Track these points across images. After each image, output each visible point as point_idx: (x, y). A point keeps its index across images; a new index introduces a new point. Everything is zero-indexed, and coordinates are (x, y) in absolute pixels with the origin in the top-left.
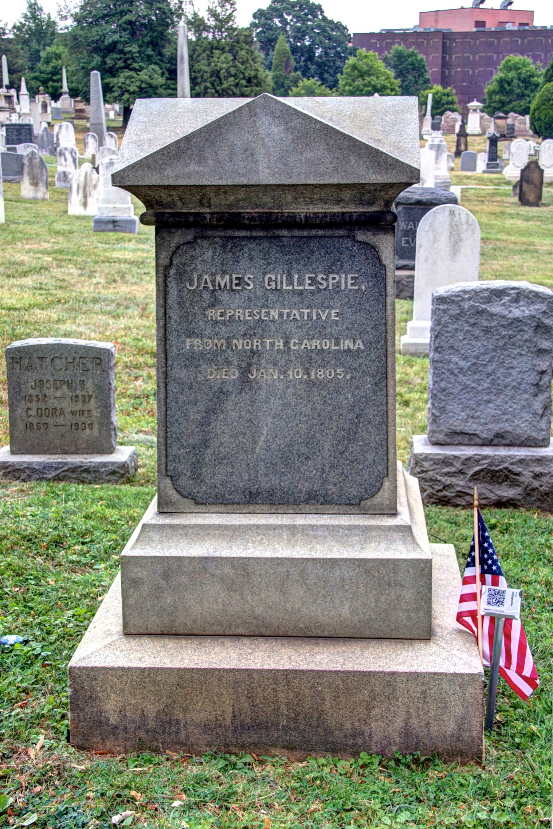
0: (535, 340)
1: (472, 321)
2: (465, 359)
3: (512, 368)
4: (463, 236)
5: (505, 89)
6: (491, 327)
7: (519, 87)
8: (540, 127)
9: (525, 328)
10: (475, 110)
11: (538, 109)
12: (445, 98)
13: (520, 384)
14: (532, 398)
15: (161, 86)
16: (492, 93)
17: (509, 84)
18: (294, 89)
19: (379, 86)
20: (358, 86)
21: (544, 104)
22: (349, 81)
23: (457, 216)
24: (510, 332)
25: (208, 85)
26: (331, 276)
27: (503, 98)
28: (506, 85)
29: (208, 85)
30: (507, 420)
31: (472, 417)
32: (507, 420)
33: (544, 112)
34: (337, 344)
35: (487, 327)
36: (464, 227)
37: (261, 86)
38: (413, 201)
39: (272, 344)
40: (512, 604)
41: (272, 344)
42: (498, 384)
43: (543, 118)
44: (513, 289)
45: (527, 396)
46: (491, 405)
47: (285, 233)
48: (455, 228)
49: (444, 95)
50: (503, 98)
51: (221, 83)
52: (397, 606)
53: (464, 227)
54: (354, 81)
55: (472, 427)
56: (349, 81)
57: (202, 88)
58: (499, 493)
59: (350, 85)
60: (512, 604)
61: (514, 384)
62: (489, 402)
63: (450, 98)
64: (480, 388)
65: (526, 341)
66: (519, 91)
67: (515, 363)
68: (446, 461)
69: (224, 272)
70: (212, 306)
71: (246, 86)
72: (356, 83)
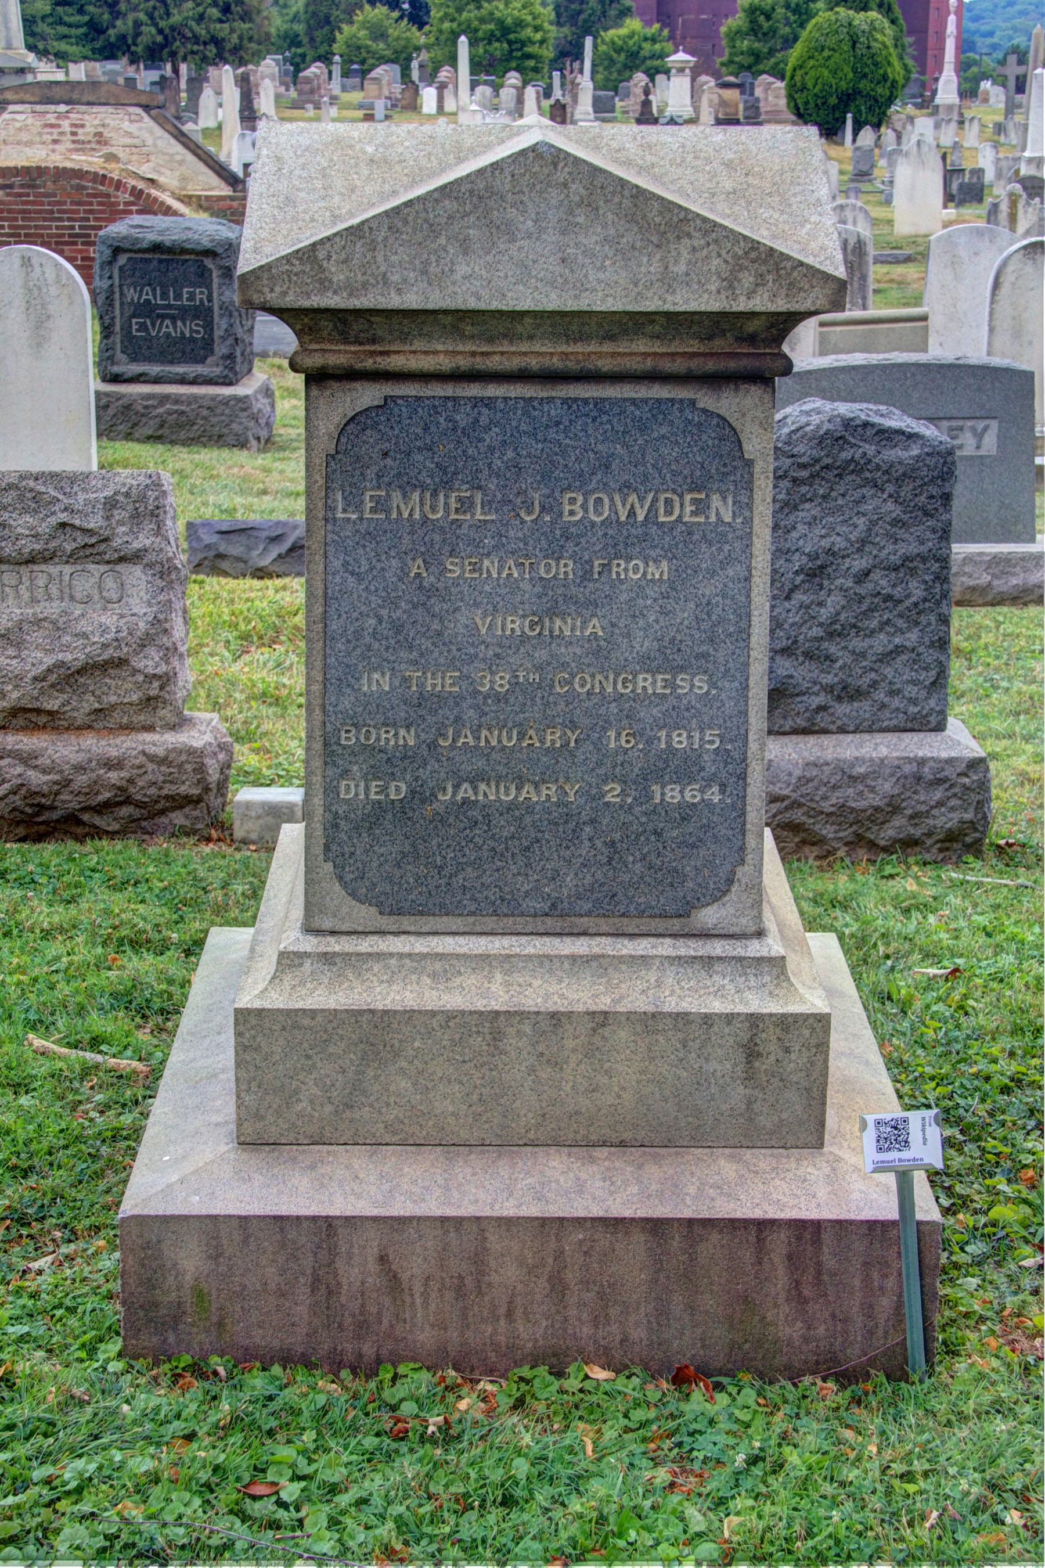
4: (52, 308)
5: (761, 27)
7: (788, 23)
8: (807, 103)
10: (681, 70)
11: (801, 67)
12: (647, 46)
15: (44, 18)
16: (735, 35)
17: (768, 18)
18: (345, 27)
19: (509, 20)
20: (469, 21)
21: (811, 57)
22: (451, 10)
23: (38, 270)
25: (142, 16)
27: (756, 45)
28: (762, 18)
29: (142, 16)
33: (812, 73)
36: (54, 291)
37: (251, 20)
38: (145, 245)
43: (810, 85)
48: (36, 292)
49: (646, 39)
50: (756, 45)
51: (168, 14)
52: (775, 1079)
53: (54, 291)
54: (459, 10)
56: (451, 10)
57: (130, 23)
59: (452, 20)
63: (657, 46)
66: (787, 30)
71: (221, 21)
72: (465, 14)
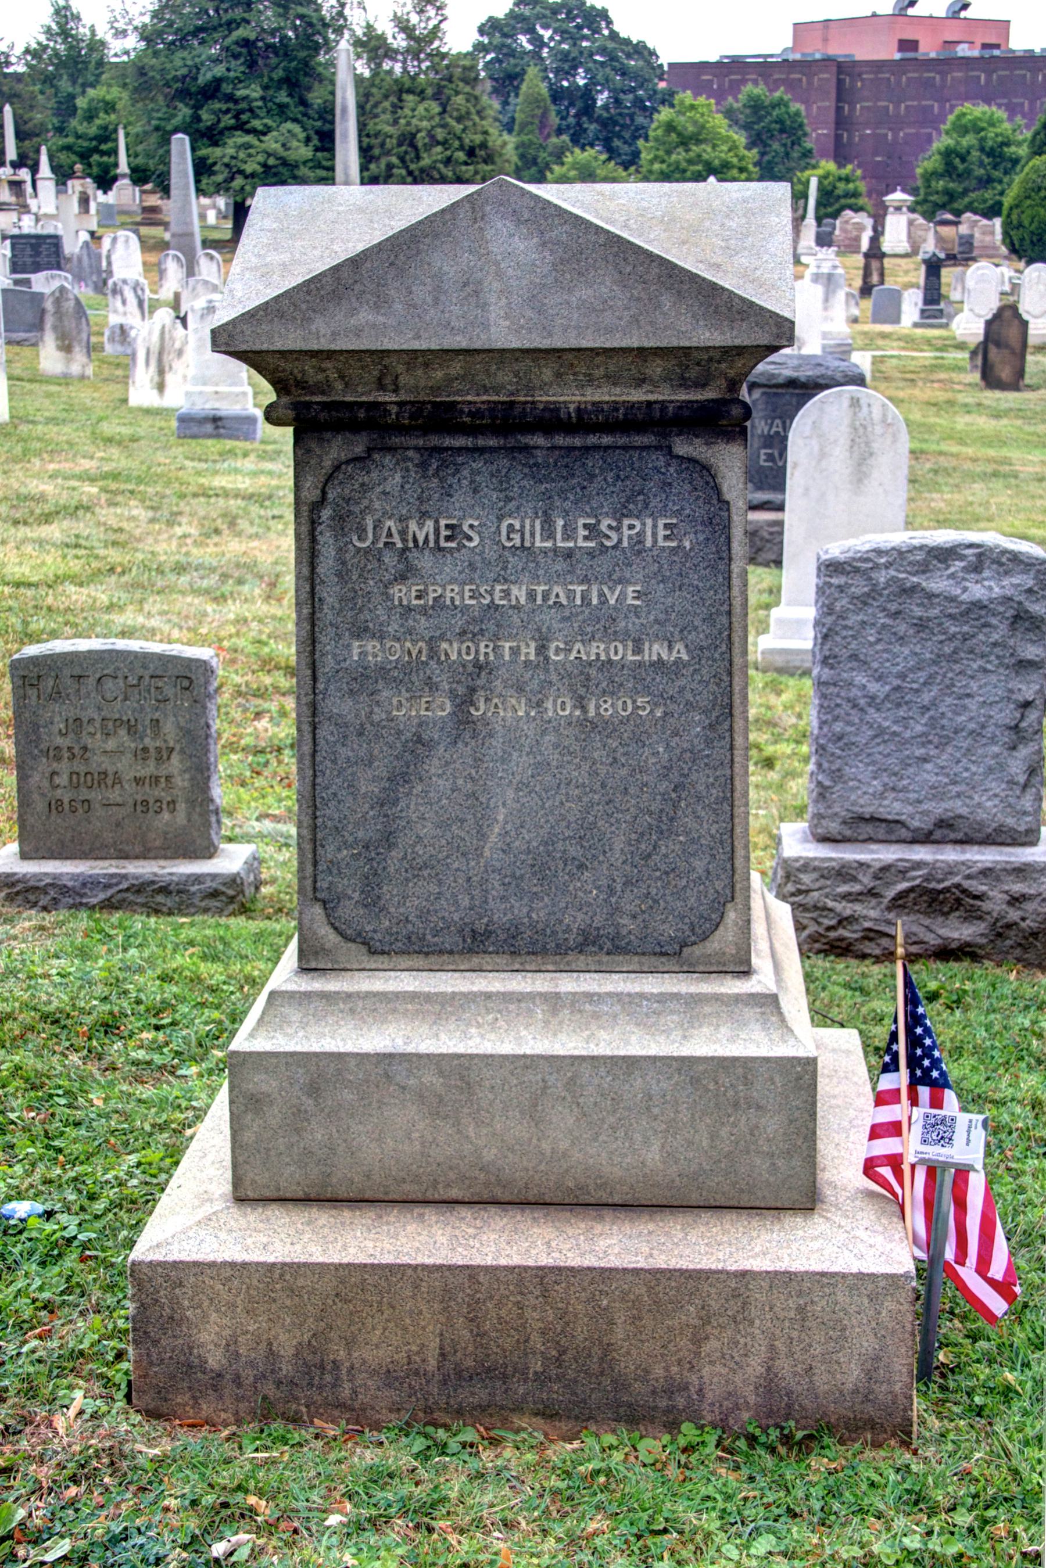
0: (1011, 642)
1: (893, 607)
2: (879, 679)
3: (968, 695)
4: (875, 446)
5: (955, 168)
6: (929, 619)
7: (981, 164)
8: (1022, 240)
9: (994, 621)
10: (898, 209)
11: (1017, 206)
12: (841, 186)
13: (983, 727)
14: (1006, 753)
15: (305, 163)
16: (930, 176)
17: (963, 160)
18: (556, 168)
19: (717, 162)
20: (678, 163)
21: (1028, 197)
22: (661, 153)
23: (865, 409)
24: (965, 628)
25: (394, 160)
26: (626, 522)
27: (951, 185)
28: (957, 161)
29: (394, 160)
30: (958, 795)
31: (893, 789)
32: (958, 795)
33: (1029, 212)
34: (638, 650)
35: (920, 619)
36: (879, 429)
37: (493, 163)
38: (781, 380)
39: (515, 651)
41: (515, 651)
42: (943, 727)
43: (1026, 223)
44: (971, 546)
45: (996, 749)
46: (929, 766)
47: (539, 440)
48: (861, 431)
49: (840, 179)
50: (951, 185)
51: (418, 158)
52: (752, 1146)
53: (879, 429)
54: (669, 153)
55: (893, 807)
56: (661, 153)
57: (383, 166)
58: (944, 932)
59: (663, 162)
61: (972, 726)
62: (925, 760)
63: (851, 186)
64: (908, 734)
65: (995, 644)
66: (982, 171)
67: (974, 686)
68: (843, 873)
69: (424, 515)
70: (401, 578)
71: (466, 164)
72: (674, 157)
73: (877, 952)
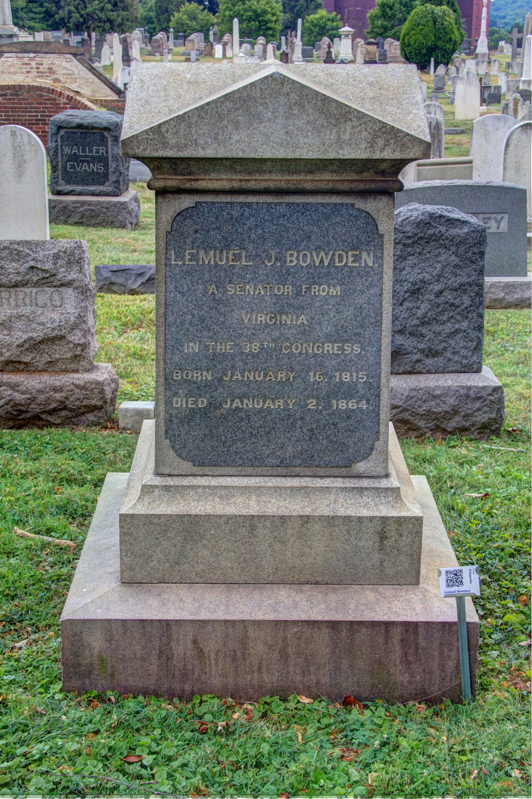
4: (26, 157)
5: (387, 14)
7: (401, 12)
8: (411, 52)
10: (347, 36)
11: (408, 34)
12: (329, 23)
15: (22, 9)
16: (374, 18)
17: (391, 9)
18: (176, 14)
19: (259, 10)
20: (239, 11)
21: (413, 29)
22: (230, 5)
23: (19, 138)
25: (72, 8)
27: (385, 23)
28: (388, 9)
29: (72, 8)
33: (413, 37)
36: (27, 148)
37: (128, 10)
38: (74, 125)
40: (471, 581)
43: (412, 43)
48: (18, 149)
49: (329, 20)
50: (385, 23)
51: (86, 7)
52: (394, 550)
53: (27, 148)
54: (234, 5)
56: (230, 5)
57: (66, 12)
59: (230, 10)
60: (471, 581)
63: (335, 24)
66: (401, 15)
71: (112, 11)
72: (237, 7)
73: (59, 421)
